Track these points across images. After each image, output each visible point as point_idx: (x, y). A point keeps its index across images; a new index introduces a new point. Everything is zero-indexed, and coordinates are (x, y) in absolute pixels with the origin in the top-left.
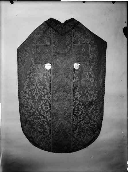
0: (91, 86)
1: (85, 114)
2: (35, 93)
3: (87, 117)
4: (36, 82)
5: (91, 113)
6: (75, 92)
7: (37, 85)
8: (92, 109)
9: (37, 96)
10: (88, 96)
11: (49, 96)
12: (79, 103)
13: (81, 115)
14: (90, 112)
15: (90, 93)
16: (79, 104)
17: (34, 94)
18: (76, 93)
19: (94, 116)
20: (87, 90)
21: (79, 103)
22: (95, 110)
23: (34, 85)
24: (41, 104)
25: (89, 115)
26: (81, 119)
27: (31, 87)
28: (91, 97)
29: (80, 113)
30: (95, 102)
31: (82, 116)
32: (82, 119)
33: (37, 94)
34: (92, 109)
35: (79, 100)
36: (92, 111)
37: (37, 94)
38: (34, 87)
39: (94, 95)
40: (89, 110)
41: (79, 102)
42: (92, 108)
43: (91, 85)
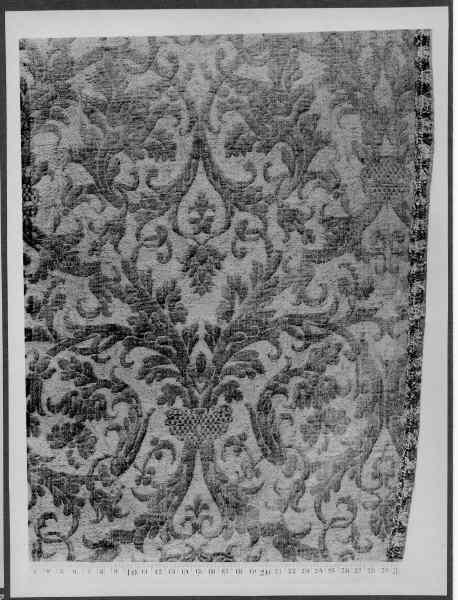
0: (238, 83)
1: (179, 446)
2: (180, 247)
3: (199, 489)
4: (190, 105)
5: (252, 442)
6: (45, 169)
7: (200, 147)
8: (260, 383)
9: (202, 286)
10: (219, 217)
11: (364, 272)
12: (92, 303)
13: (123, 469)
14: (234, 430)
15: (233, 170)
16: (100, 321)
17: (174, 268)
18: (60, 181)
19: (287, 485)
20: (199, 142)
21: (102, 310)
22: (302, 400)
23: (164, 150)
24: (252, 389)
25: (230, 465)
26: (114, 514)
27: (124, 178)
28: (255, 223)
29: (108, 444)
30: (302, 298)
31: (131, 475)
32: (128, 525)
33: (201, 264)
34: (260, 383)
35: (94, 268)
36: (264, 407)
37: (201, 264)
38: (175, 169)
39: (292, 201)
40: (235, 395)
41: (96, 290)
42: (273, 370)
43: (242, 71)
